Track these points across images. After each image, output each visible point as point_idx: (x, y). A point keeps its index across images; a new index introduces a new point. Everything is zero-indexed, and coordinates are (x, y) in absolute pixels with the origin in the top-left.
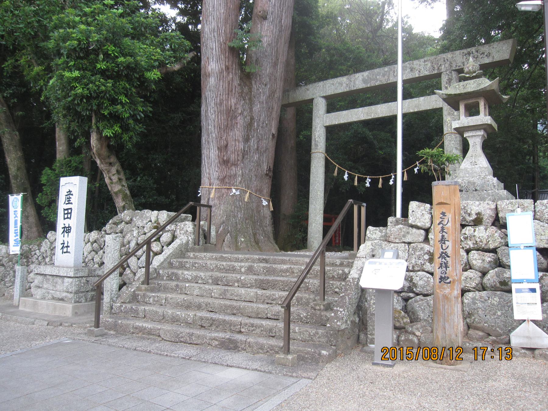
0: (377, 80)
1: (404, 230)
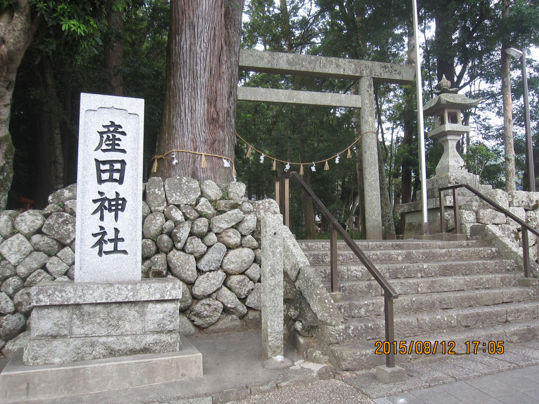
0: (303, 66)
1: (493, 213)
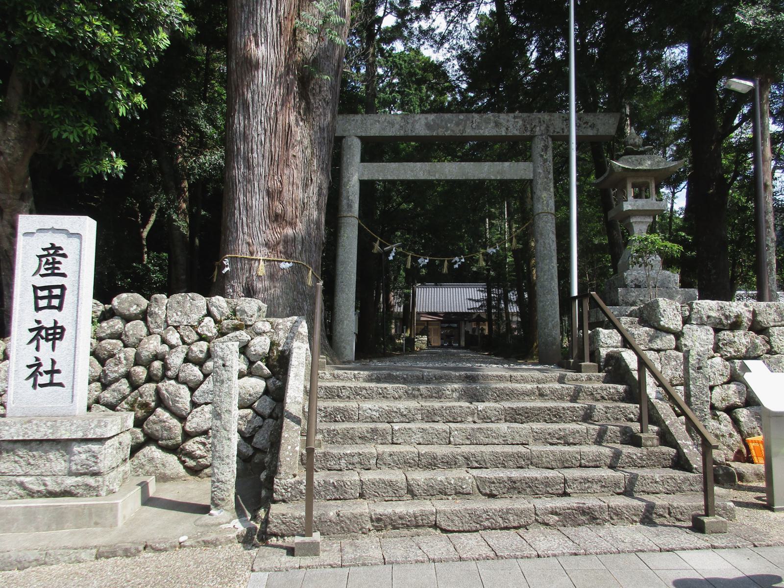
0: (447, 129)
